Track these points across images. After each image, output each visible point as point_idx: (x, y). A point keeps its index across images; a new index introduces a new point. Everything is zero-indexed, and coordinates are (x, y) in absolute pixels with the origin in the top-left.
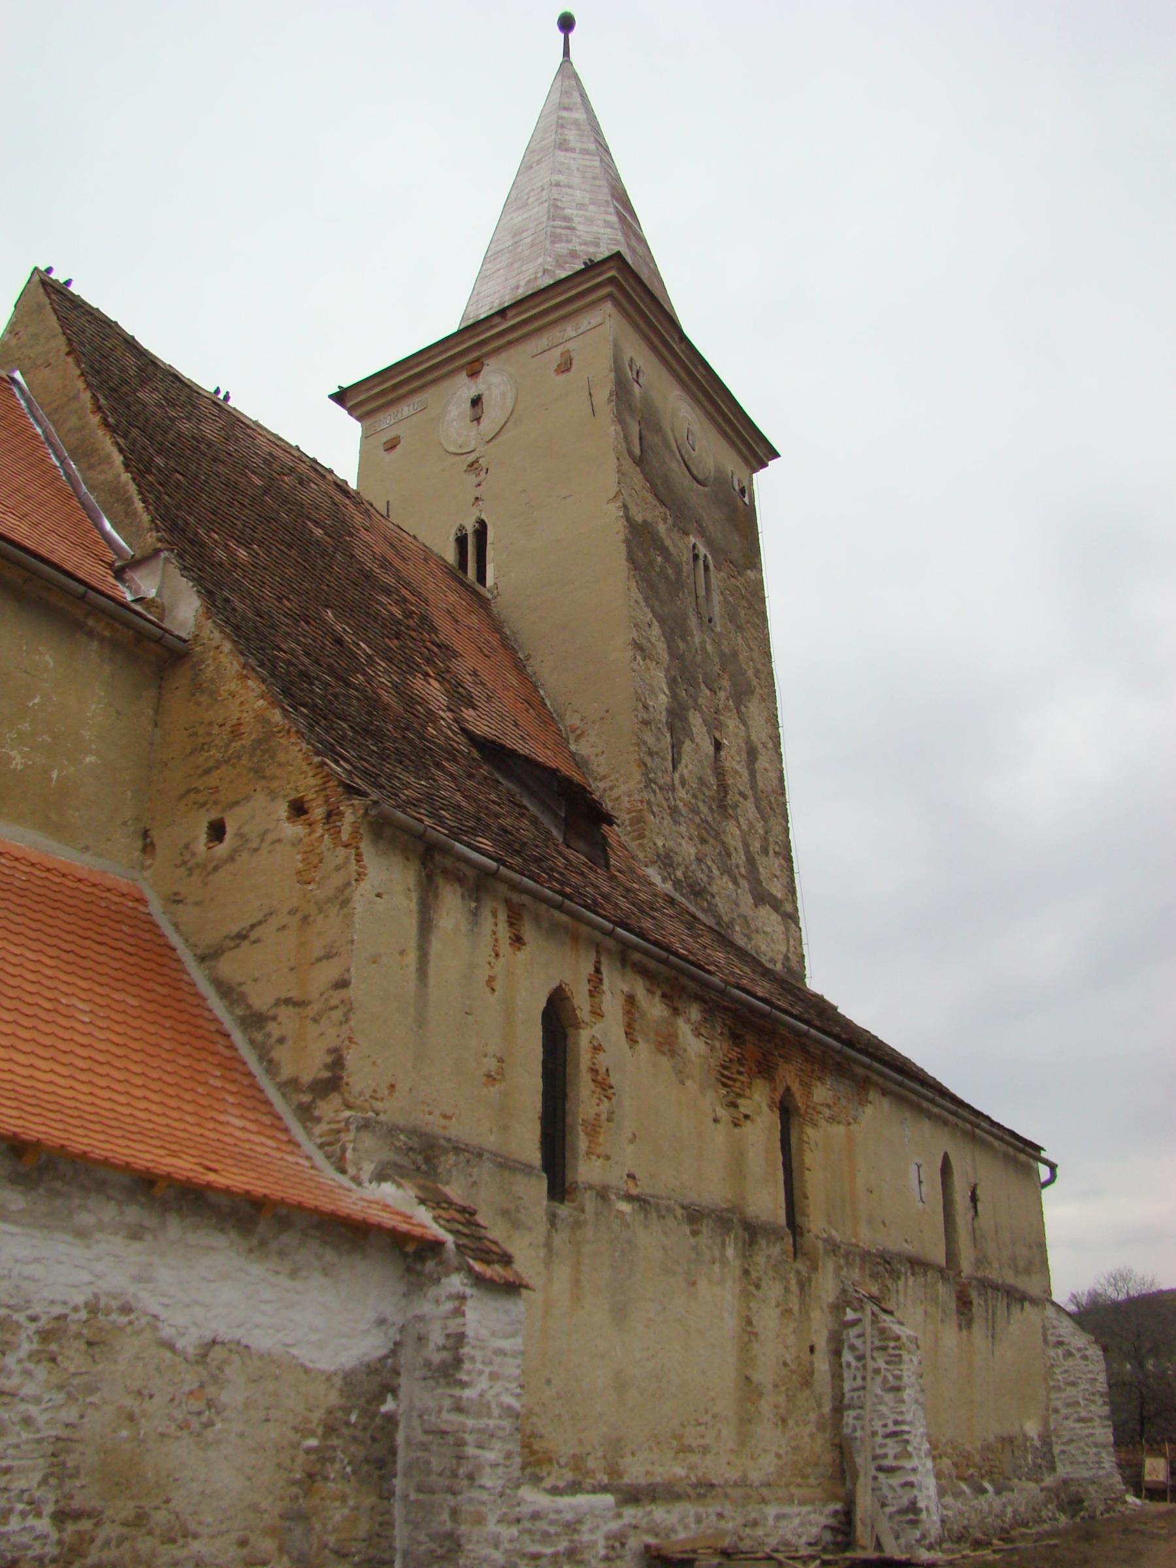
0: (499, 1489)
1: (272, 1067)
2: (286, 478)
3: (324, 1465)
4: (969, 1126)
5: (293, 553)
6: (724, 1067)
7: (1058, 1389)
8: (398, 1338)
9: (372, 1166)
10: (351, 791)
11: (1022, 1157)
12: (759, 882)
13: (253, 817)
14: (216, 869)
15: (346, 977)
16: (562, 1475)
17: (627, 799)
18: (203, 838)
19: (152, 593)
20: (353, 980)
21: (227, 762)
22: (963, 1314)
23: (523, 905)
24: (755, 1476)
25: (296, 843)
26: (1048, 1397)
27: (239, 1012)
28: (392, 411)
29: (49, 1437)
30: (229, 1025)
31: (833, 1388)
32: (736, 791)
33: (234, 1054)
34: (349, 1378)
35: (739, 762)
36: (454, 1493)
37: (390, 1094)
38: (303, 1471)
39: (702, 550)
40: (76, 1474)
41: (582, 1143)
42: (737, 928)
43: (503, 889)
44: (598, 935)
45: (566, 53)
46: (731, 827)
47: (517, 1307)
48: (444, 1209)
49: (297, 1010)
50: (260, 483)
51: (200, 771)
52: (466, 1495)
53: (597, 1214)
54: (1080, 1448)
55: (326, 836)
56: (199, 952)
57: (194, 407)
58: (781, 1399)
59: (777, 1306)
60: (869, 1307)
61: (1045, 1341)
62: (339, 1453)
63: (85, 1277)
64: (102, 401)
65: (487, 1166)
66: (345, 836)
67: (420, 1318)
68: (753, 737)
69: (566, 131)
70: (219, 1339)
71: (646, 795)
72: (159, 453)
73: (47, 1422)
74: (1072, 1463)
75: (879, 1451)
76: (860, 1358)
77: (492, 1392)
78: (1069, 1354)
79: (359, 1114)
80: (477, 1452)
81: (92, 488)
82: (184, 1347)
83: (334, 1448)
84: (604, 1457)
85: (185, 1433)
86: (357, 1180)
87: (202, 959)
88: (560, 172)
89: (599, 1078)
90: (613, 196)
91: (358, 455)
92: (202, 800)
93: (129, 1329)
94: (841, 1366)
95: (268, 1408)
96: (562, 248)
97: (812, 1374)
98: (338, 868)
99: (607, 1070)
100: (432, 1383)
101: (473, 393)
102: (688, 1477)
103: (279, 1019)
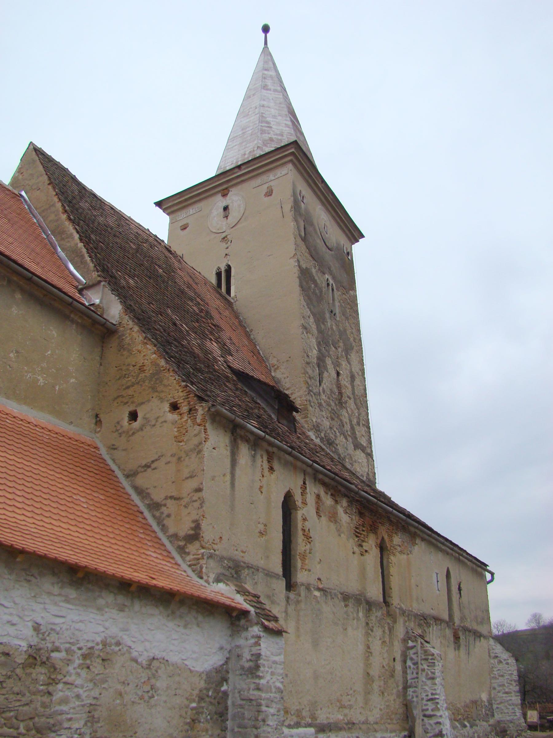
0: (275, 726)
1: (164, 528)
2: (145, 245)
3: (199, 715)
4: (457, 555)
5: (152, 281)
6: (357, 528)
7: (495, 678)
8: (228, 655)
9: (214, 576)
10: (201, 399)
11: (479, 569)
13: (152, 410)
14: (133, 434)
15: (201, 487)
16: (293, 719)
17: (299, 399)
18: (126, 419)
19: (97, 301)
20: (204, 488)
21: (138, 383)
22: (456, 643)
23: (274, 453)
24: (371, 719)
25: (174, 423)
26: (491, 683)
27: (147, 502)
28: (184, 211)
29: (88, 703)
30: (143, 508)
31: (403, 678)
32: (346, 395)
33: (147, 522)
34: (208, 674)
35: (347, 382)
36: (256, 728)
37: (220, 542)
38: (191, 718)
39: (331, 282)
40: (98, 722)
41: (299, 564)
42: (347, 460)
43: (265, 445)
44: (304, 466)
45: (266, 43)
46: (344, 412)
47: (281, 641)
48: (247, 595)
49: (176, 501)
50: (134, 247)
51: (124, 387)
52: (261, 729)
53: (306, 597)
54: (506, 706)
55: (189, 420)
56: (125, 473)
57: (103, 210)
58: (382, 683)
59: (380, 639)
60: (420, 640)
61: (490, 656)
62: (205, 710)
63: (102, 629)
64: (67, 208)
65: (261, 575)
66: (198, 421)
67: (238, 647)
68: (353, 370)
69: (266, 81)
70: (156, 657)
71: (309, 398)
72: (92, 232)
73: (86, 697)
74: (502, 713)
75: (424, 707)
76: (415, 664)
77: (272, 681)
78: (500, 662)
79: (208, 551)
80: (266, 709)
81: (63, 250)
82: (142, 661)
83: (203, 707)
84: (309, 710)
85: (142, 701)
86: (207, 581)
87: (127, 476)
88: (264, 100)
89: (306, 534)
90: (289, 112)
91: (168, 231)
92: (126, 401)
93: (119, 653)
94: (406, 668)
95: (176, 689)
96: (266, 136)
97: (394, 671)
98: (196, 435)
99: (309, 530)
100: (245, 677)
101: (224, 204)
102: (343, 720)
103: (167, 506)
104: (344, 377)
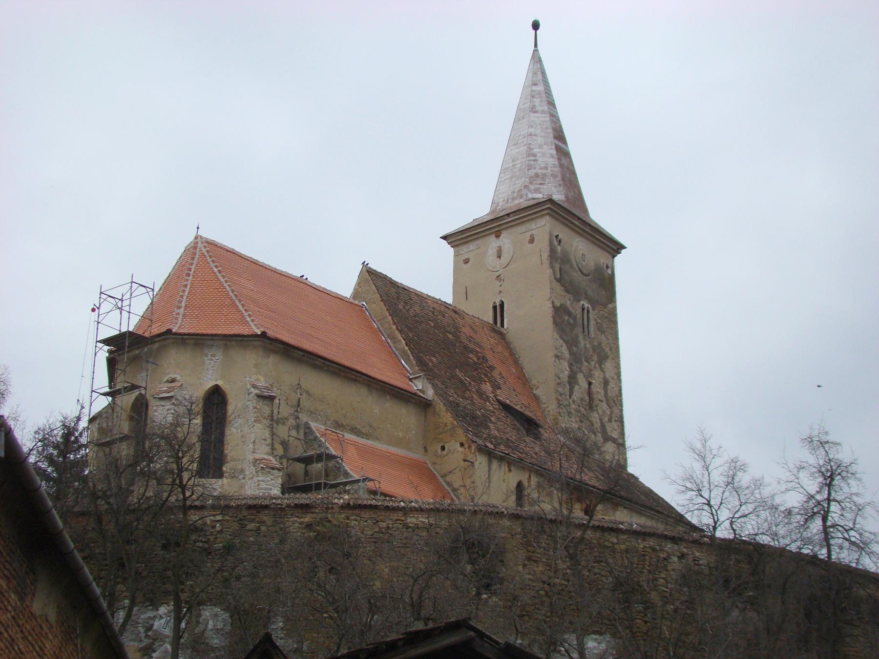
12: (606, 433)
14: (444, 457)
18: (440, 450)
19: (421, 388)
25: (462, 452)
28: (466, 246)
30: (450, 491)
39: (586, 305)
45: (536, 45)
46: (595, 414)
66: (473, 451)
68: (607, 376)
81: (397, 349)
87: (442, 477)
88: (532, 127)
96: (532, 172)
101: (498, 245)
104: (597, 385)
